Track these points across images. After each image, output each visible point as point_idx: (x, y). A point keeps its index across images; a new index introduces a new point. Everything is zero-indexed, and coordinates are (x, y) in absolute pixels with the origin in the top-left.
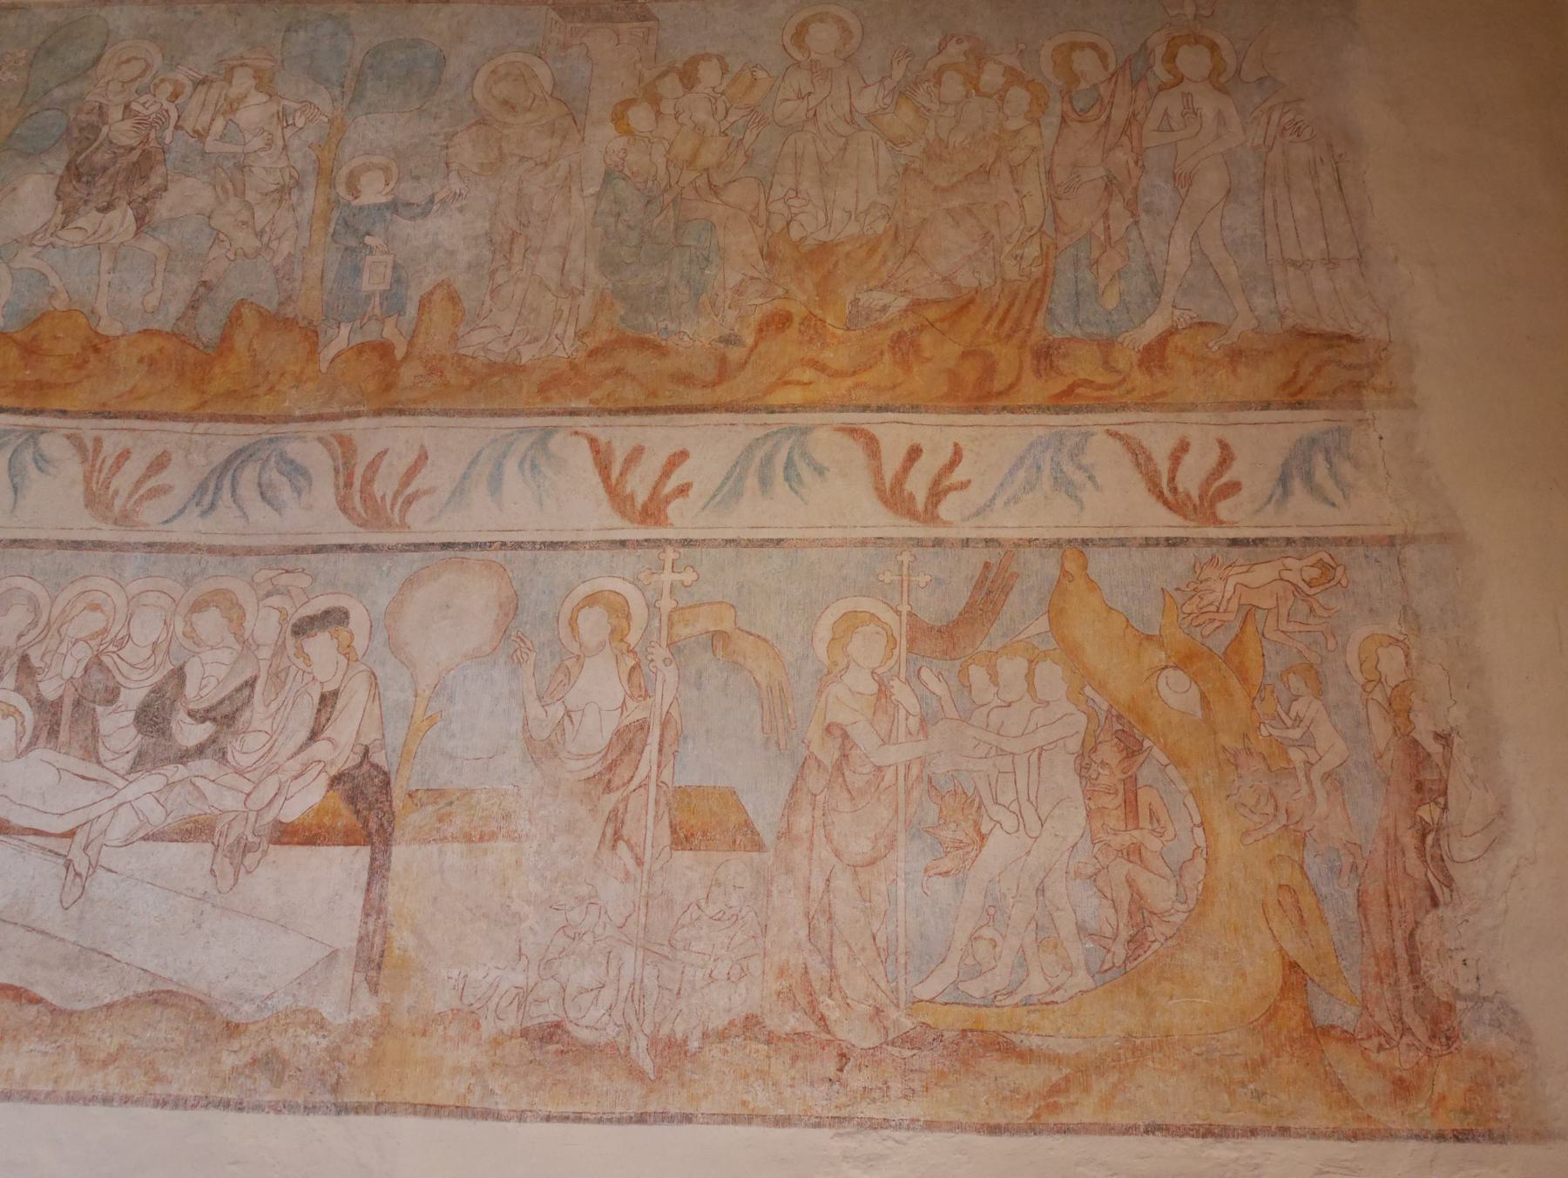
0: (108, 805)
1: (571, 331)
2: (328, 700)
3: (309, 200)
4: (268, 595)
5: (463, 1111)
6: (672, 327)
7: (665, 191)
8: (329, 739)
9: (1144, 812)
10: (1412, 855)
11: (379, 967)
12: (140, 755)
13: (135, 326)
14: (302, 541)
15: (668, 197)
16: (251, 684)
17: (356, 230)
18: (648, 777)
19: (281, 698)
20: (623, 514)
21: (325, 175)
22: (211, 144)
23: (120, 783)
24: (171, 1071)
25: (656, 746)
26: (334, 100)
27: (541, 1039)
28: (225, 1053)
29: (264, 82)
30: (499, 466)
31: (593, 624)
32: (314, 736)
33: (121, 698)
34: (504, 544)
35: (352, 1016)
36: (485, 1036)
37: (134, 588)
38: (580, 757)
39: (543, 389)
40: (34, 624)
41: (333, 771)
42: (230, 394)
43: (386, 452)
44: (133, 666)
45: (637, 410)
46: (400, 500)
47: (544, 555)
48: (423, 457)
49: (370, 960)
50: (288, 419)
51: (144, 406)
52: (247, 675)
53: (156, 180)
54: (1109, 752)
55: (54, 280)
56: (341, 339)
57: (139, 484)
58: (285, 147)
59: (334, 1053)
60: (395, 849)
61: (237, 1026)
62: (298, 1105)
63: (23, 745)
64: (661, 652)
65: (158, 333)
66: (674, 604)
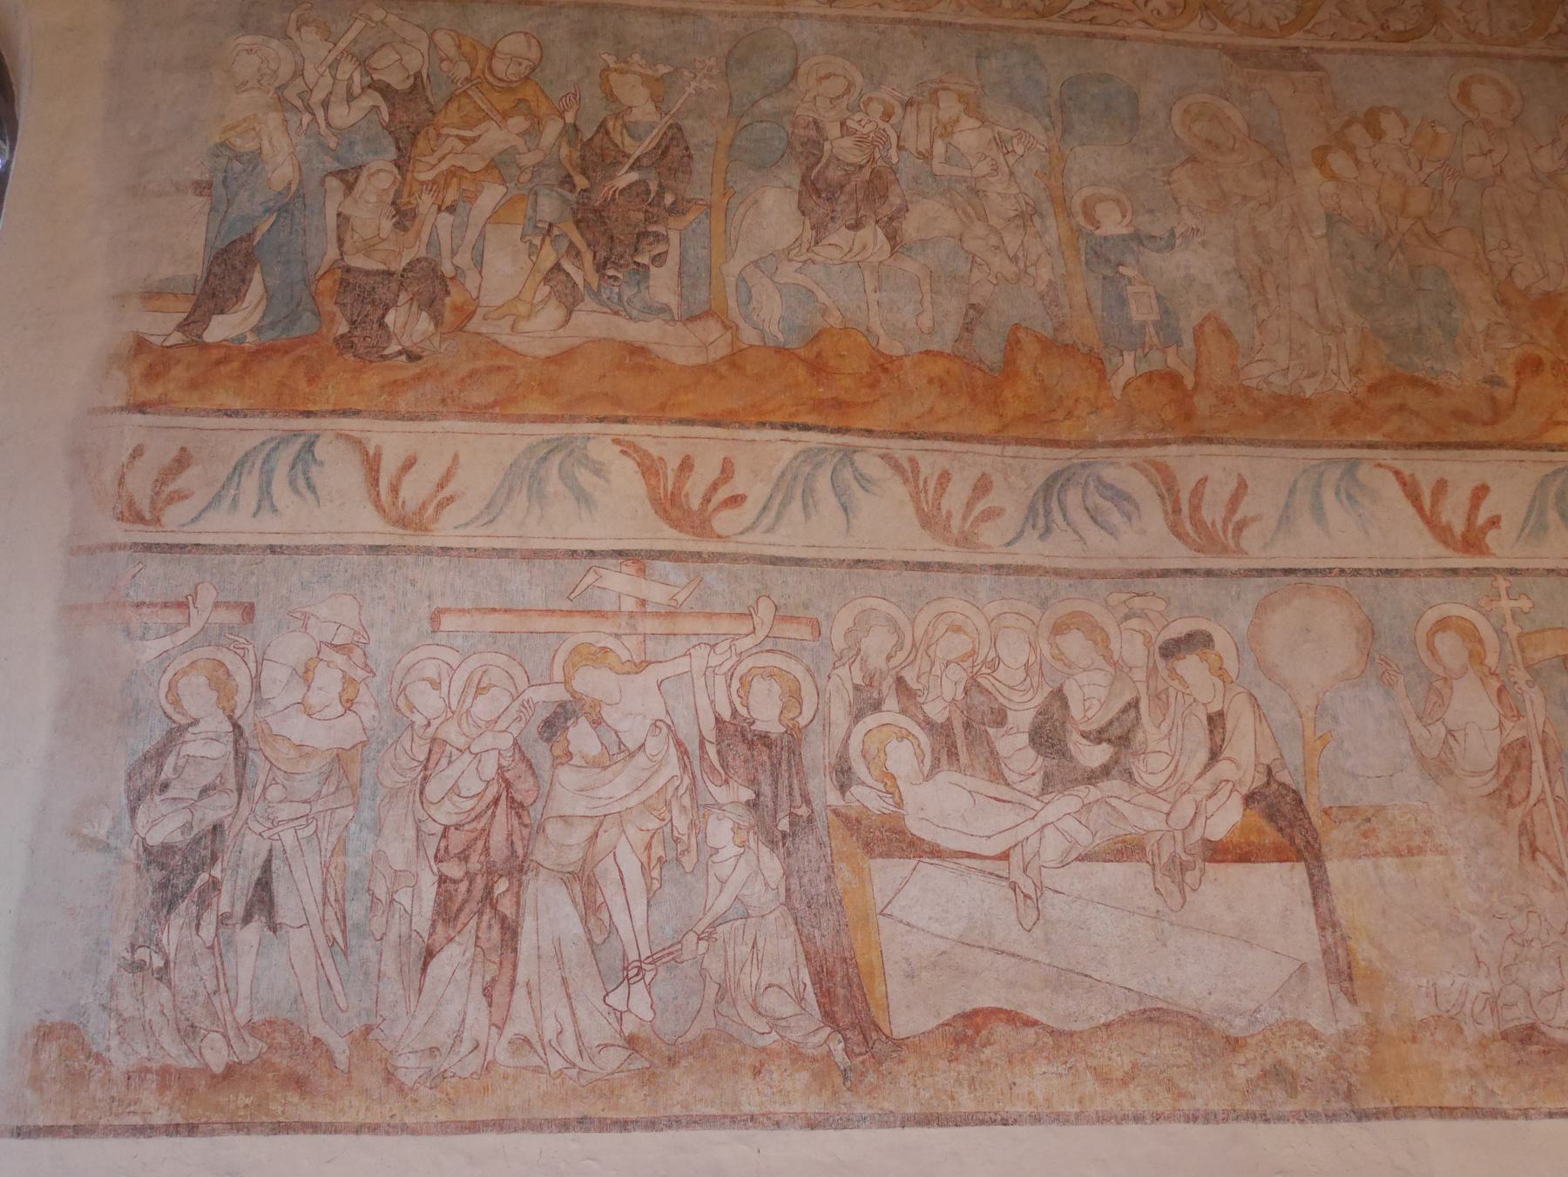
0: (1030, 828)
1: (1344, 368)
2: (1216, 721)
3: (1053, 229)
4: (1127, 617)
5: (1473, 1112)
6: (1438, 366)
7: (1387, 237)
8: (1229, 759)
11: (1351, 978)
12: (1047, 776)
13: (916, 347)
14: (1145, 565)
15: (1393, 243)
16: (1134, 704)
17: (1108, 261)
18: (1543, 791)
19: (1168, 720)
20: (1446, 543)
21: (1061, 204)
22: (937, 167)
23: (1038, 805)
24: (1192, 1086)
25: (1542, 764)
26: (1047, 130)
27: (1521, 1041)
28: (1235, 1067)
29: (972, 107)
30: (1317, 495)
31: (1448, 645)
32: (1214, 756)
33: (1010, 719)
34: (1342, 571)
35: (1341, 1026)
36: (1470, 1040)
37: (993, 609)
38: (1475, 774)
39: (1337, 421)
40: (899, 646)
41: (1245, 790)
42: (1028, 418)
43: (1206, 479)
44: (1012, 688)
45: (1430, 445)
46: (1230, 527)
47: (1383, 582)
48: (1242, 486)
49: (1340, 972)
50: (1094, 445)
51: (942, 428)
52: (1128, 697)
53: (896, 201)
55: (822, 296)
56: (1126, 368)
57: (969, 506)
58: (1012, 174)
59: (1335, 1060)
60: (1329, 866)
61: (1237, 1040)
62: (1318, 1114)
63: (927, 768)
64: (1521, 675)
65: (941, 354)
66: (1518, 630)
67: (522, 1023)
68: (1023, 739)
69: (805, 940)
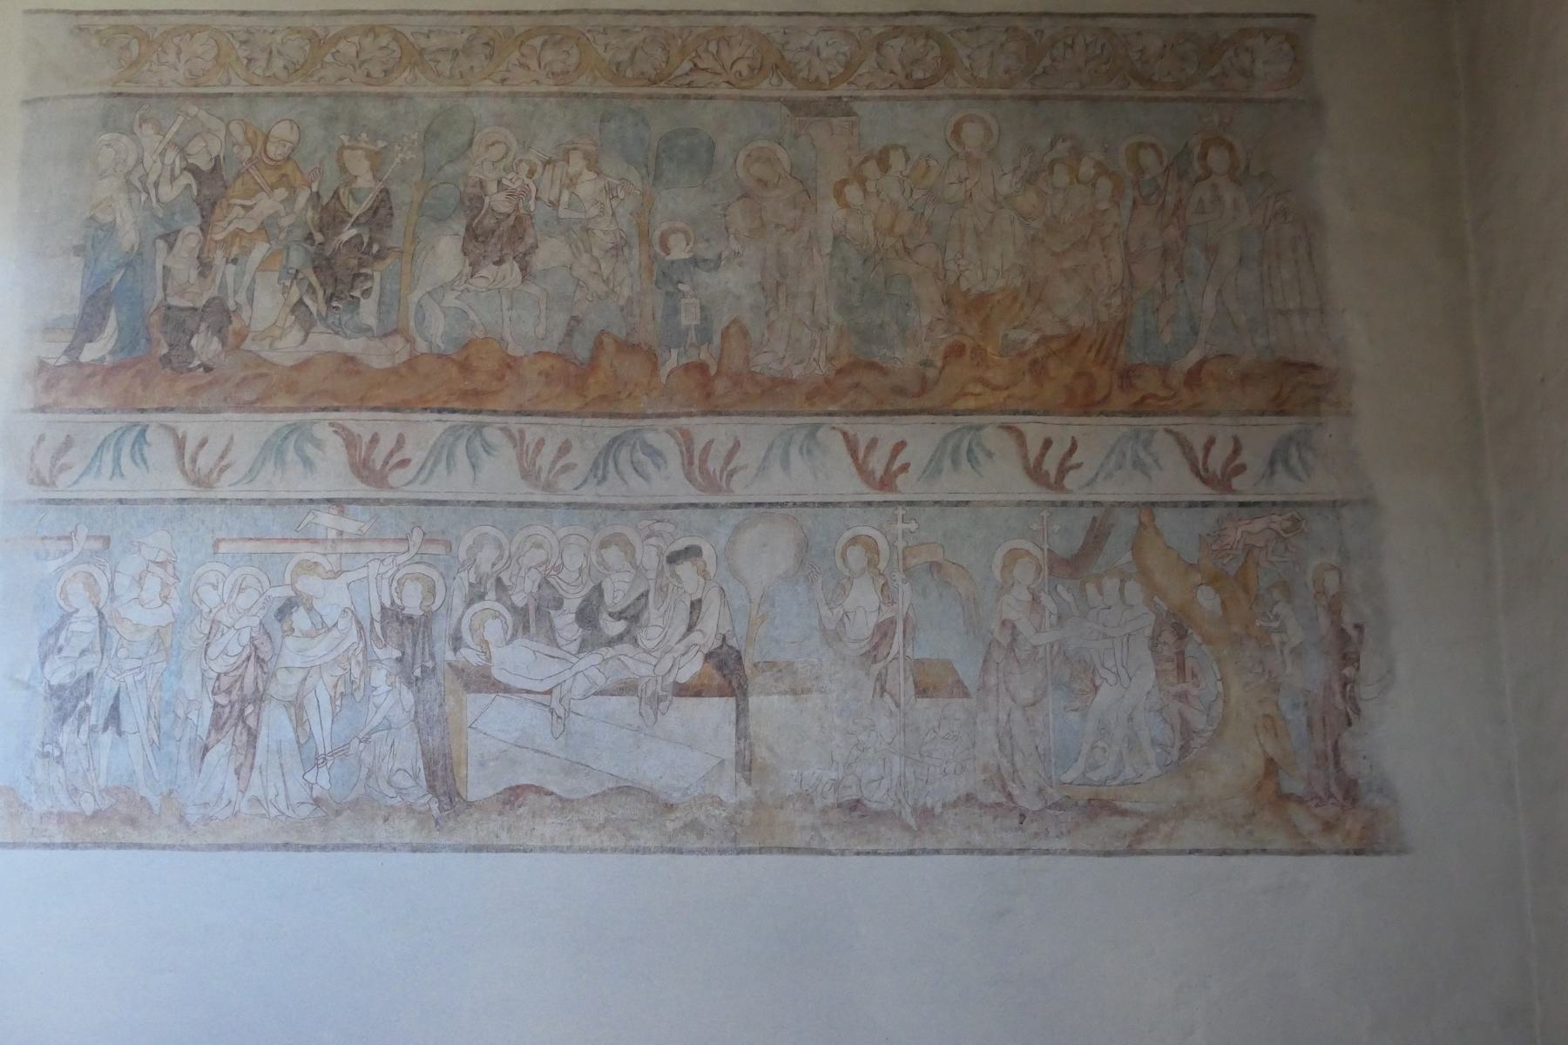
9: (1188, 672)
10: (1338, 697)
54: (1168, 637)
67: (255, 791)
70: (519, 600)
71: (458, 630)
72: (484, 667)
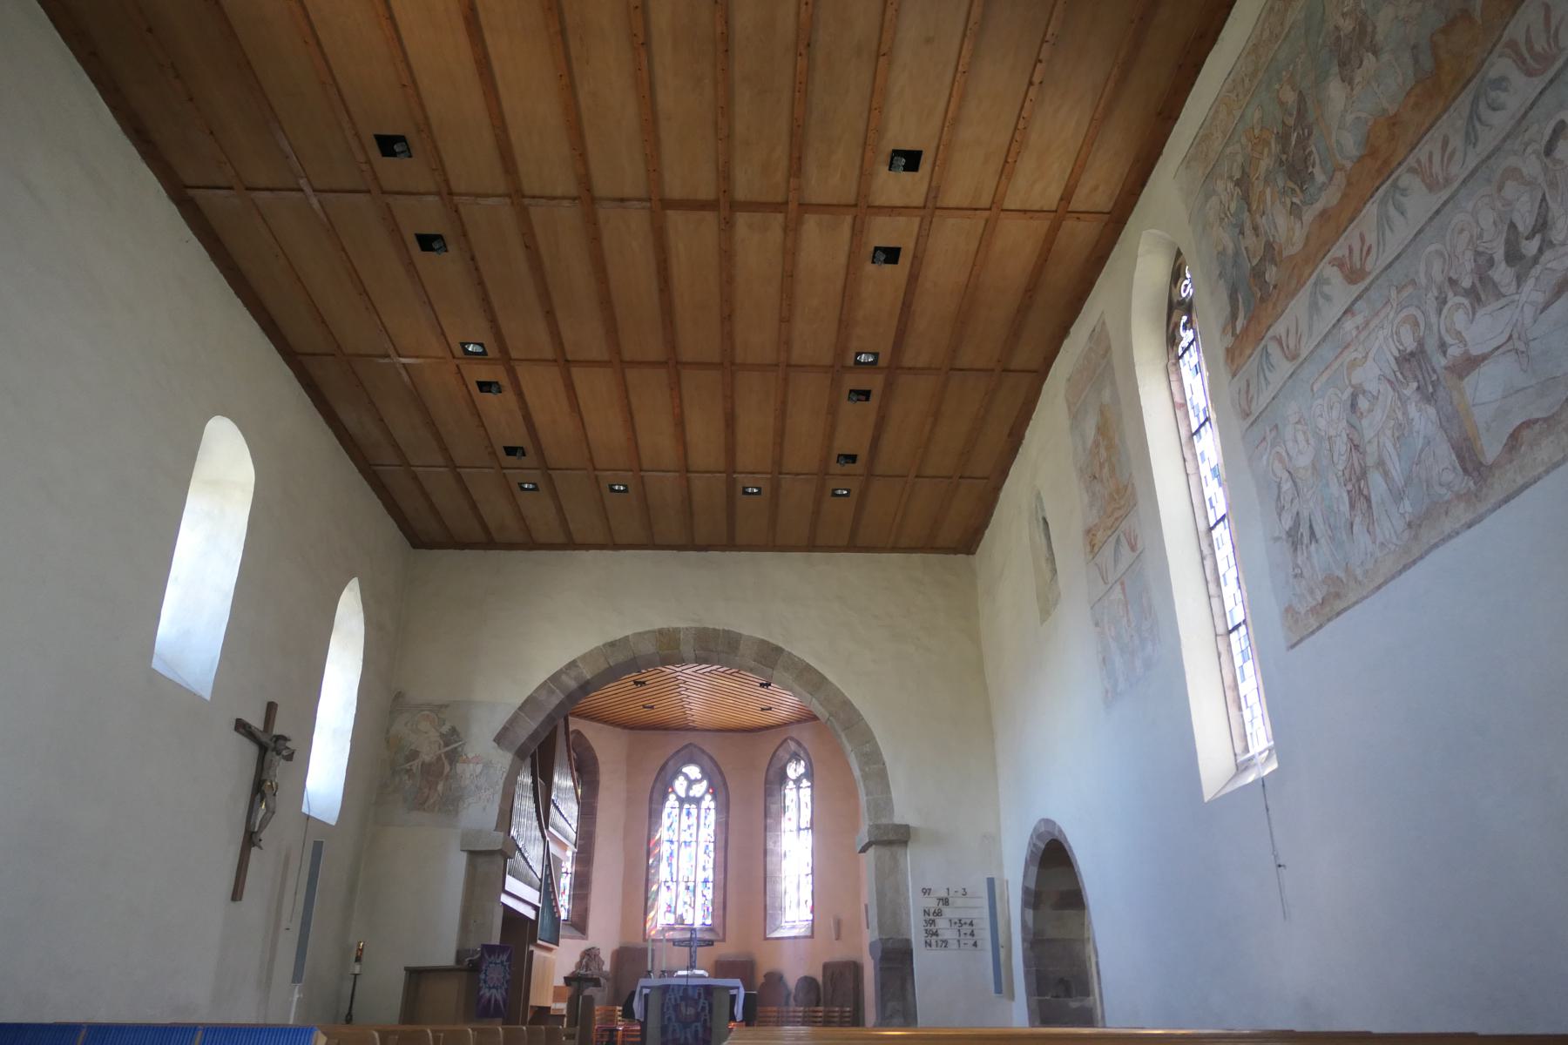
67: (1380, 539)
68: (1503, 265)
69: (1450, 439)
70: (1466, 283)
71: (1441, 338)
72: (1466, 352)
